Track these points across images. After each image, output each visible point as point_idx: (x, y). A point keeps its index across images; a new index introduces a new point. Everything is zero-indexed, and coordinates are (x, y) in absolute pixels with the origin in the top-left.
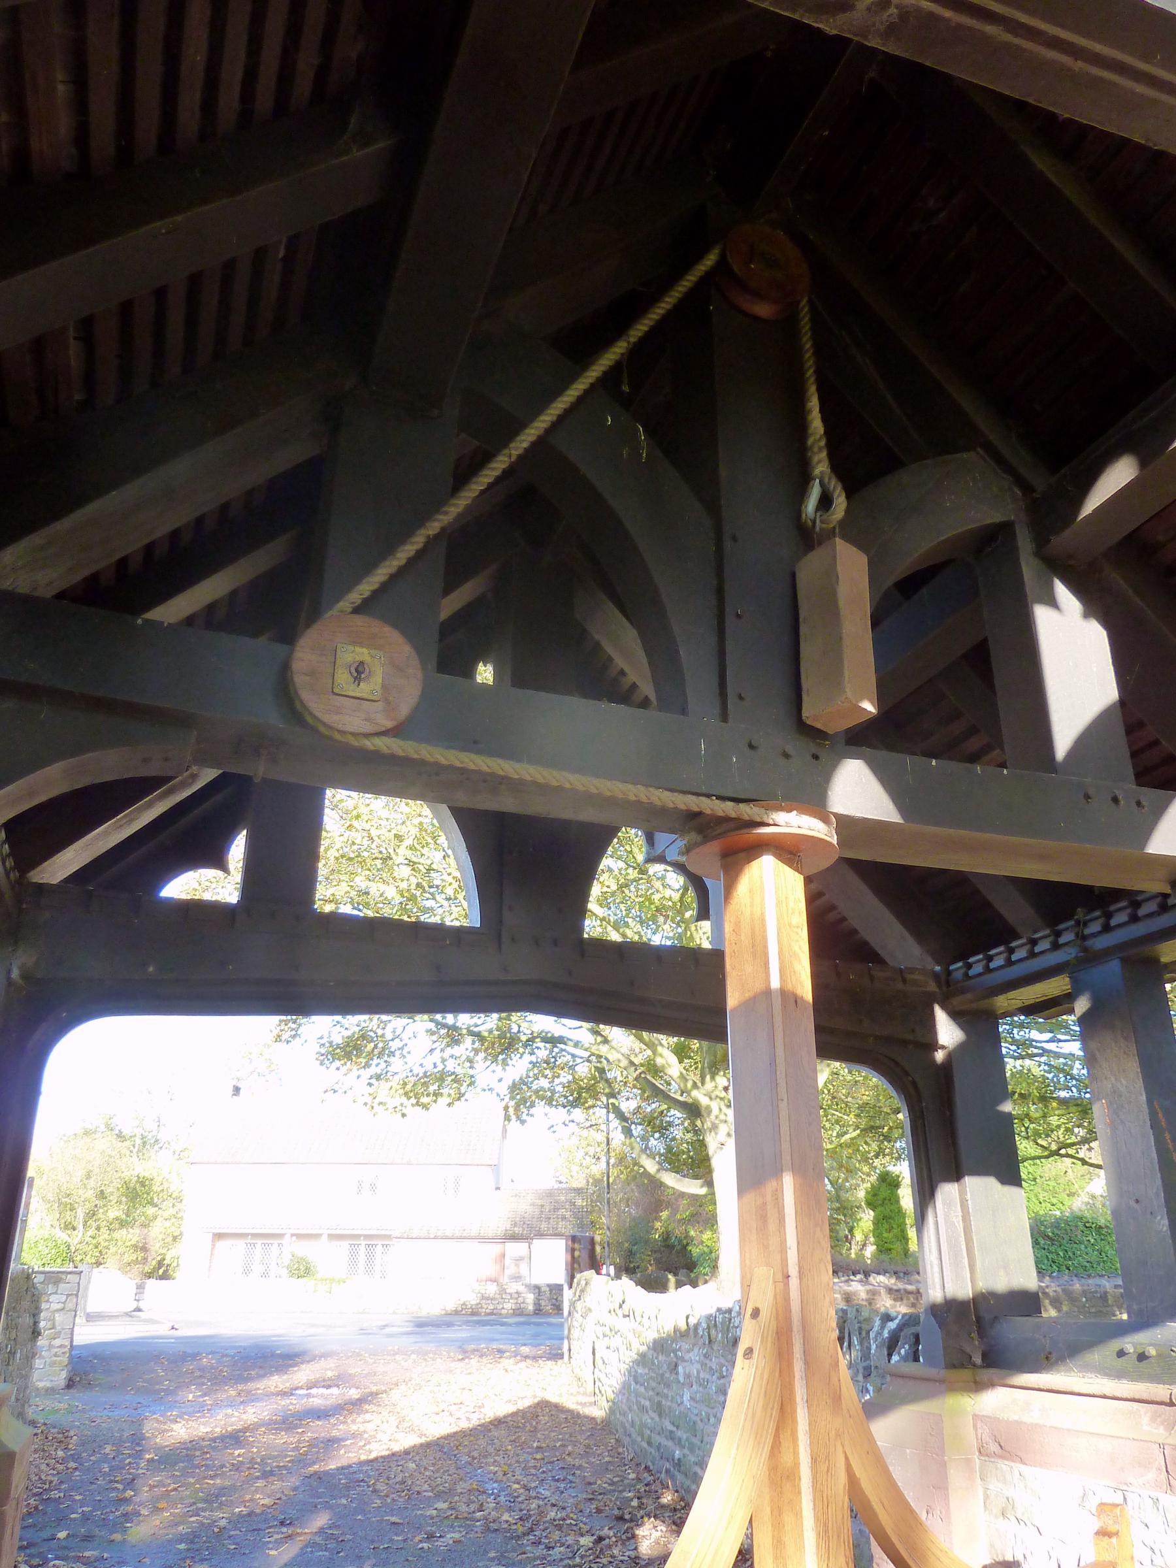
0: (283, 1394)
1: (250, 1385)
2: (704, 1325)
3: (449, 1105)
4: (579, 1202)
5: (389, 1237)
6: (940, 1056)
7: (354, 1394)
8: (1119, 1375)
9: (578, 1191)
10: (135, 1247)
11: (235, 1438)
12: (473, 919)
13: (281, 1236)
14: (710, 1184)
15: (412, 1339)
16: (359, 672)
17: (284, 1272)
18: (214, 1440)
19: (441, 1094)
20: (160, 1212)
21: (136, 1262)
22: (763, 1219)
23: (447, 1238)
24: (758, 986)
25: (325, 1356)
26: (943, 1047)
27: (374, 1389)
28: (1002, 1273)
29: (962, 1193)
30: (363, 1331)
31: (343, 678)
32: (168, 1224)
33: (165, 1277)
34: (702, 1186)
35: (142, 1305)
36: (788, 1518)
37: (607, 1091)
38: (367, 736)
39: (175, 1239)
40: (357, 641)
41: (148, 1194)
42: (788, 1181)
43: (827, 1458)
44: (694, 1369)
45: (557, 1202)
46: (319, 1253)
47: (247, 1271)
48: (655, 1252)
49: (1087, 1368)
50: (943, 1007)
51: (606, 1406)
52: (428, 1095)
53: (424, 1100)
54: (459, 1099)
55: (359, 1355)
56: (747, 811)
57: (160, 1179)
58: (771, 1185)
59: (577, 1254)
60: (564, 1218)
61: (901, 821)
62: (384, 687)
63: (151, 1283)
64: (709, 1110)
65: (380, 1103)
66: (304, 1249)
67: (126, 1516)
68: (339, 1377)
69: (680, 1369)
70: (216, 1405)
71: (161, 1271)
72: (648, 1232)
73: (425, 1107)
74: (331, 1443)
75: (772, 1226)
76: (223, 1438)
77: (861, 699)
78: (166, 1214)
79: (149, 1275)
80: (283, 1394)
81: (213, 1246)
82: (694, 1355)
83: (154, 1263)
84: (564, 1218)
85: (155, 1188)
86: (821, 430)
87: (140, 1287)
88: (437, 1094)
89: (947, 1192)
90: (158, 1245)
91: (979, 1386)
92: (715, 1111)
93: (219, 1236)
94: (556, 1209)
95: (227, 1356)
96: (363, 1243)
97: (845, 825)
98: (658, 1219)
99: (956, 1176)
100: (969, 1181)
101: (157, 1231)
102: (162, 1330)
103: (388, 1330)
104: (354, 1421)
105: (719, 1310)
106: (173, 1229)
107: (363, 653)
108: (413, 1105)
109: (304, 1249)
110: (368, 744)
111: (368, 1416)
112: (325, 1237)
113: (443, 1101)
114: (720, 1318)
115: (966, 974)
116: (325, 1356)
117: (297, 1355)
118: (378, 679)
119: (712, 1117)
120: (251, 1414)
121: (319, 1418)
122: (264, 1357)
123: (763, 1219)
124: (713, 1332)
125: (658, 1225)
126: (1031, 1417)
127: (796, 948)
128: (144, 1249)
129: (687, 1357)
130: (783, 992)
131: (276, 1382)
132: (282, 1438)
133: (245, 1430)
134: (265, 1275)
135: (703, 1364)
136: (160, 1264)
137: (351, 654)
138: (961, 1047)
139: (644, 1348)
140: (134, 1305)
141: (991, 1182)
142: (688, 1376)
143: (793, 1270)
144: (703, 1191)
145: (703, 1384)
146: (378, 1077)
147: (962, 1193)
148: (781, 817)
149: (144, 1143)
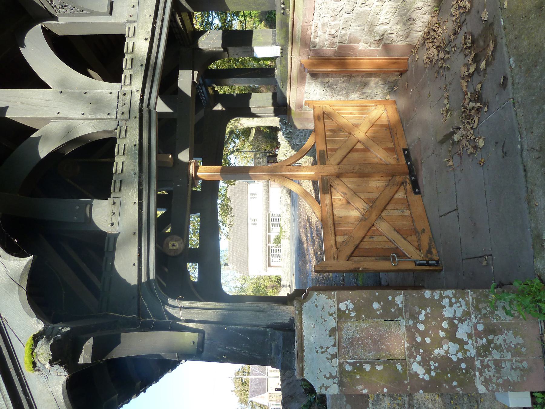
0: (308, 243)
1: (306, 252)
2: (287, 138)
3: (231, 202)
4: (258, 156)
5: (269, 215)
6: (224, 109)
7: (308, 224)
8: (286, 88)
9: (255, 156)
10: (273, 290)
11: (316, 254)
12: (199, 214)
13: (269, 247)
14: (252, 128)
15: (296, 208)
16: (173, 245)
17: (279, 245)
18: (316, 260)
19: (228, 204)
20: (263, 284)
21: (277, 289)
22: (256, 177)
23: (269, 197)
24: (219, 176)
25: (299, 232)
26: (222, 109)
27: (307, 219)
28: (269, 101)
29: (253, 107)
30: (294, 221)
31: (175, 248)
32: (266, 281)
33: (280, 280)
34: (253, 130)
35: (288, 285)
36: (296, 176)
37: (226, 156)
38: (184, 243)
39: (270, 278)
40: (168, 246)
41: (257, 288)
42: (250, 173)
43: (289, 169)
44: (297, 141)
45: (258, 163)
46: (273, 235)
47: (279, 256)
48: (273, 131)
49: (286, 92)
50: (213, 108)
51: (310, 157)
52: (228, 208)
53: (230, 209)
54: (229, 199)
55: (299, 223)
56: (190, 178)
57: (253, 285)
58: (251, 176)
59: (272, 161)
60: (263, 161)
61: (188, 149)
62: (175, 241)
63: (282, 283)
64: (231, 128)
65: (231, 223)
66: (272, 240)
67: (328, 278)
68: (304, 228)
69: (298, 144)
70: (309, 261)
71: (279, 281)
72: (267, 133)
73: (231, 209)
74: (317, 230)
75: (257, 176)
76: (316, 258)
77: (169, 158)
78: (263, 282)
79: (280, 284)
80: (308, 243)
81: (272, 267)
82: (294, 141)
83: (277, 284)
84: (263, 161)
85: (256, 286)
86: (109, 159)
87: (284, 286)
88: (228, 206)
89: (253, 110)
90: (272, 283)
91: (290, 108)
92: (231, 126)
93: (269, 265)
94: (260, 163)
95: (299, 259)
96: (271, 222)
97: (191, 158)
98: (263, 130)
99: (250, 108)
100: (250, 106)
101: (267, 284)
102: (294, 278)
103: (294, 214)
104: (313, 224)
105: (283, 135)
106: (267, 279)
107: (170, 245)
108: (231, 213)
109: (272, 240)
110: (185, 243)
111: (312, 221)
112: (269, 234)
113: (230, 204)
114: (285, 135)
115: (205, 100)
116: (299, 232)
117: (299, 240)
118: (174, 242)
119: (233, 127)
120: (312, 251)
121: (312, 234)
122: (300, 249)
123: (256, 177)
124: (288, 137)
125: (265, 130)
126: (294, 102)
127: (213, 169)
128: (273, 287)
129: (295, 142)
130: (221, 172)
131: (305, 245)
132: (316, 243)
133: (315, 252)
134: (280, 251)
135: (296, 139)
136: (277, 282)
137: (171, 247)
138: (222, 105)
139: (294, 151)
140: (288, 287)
141: (251, 100)
142: (299, 142)
143: (263, 173)
144: (254, 129)
145: (301, 139)
146: (223, 224)
147: (253, 107)
148: (191, 172)
149: (242, 291)
